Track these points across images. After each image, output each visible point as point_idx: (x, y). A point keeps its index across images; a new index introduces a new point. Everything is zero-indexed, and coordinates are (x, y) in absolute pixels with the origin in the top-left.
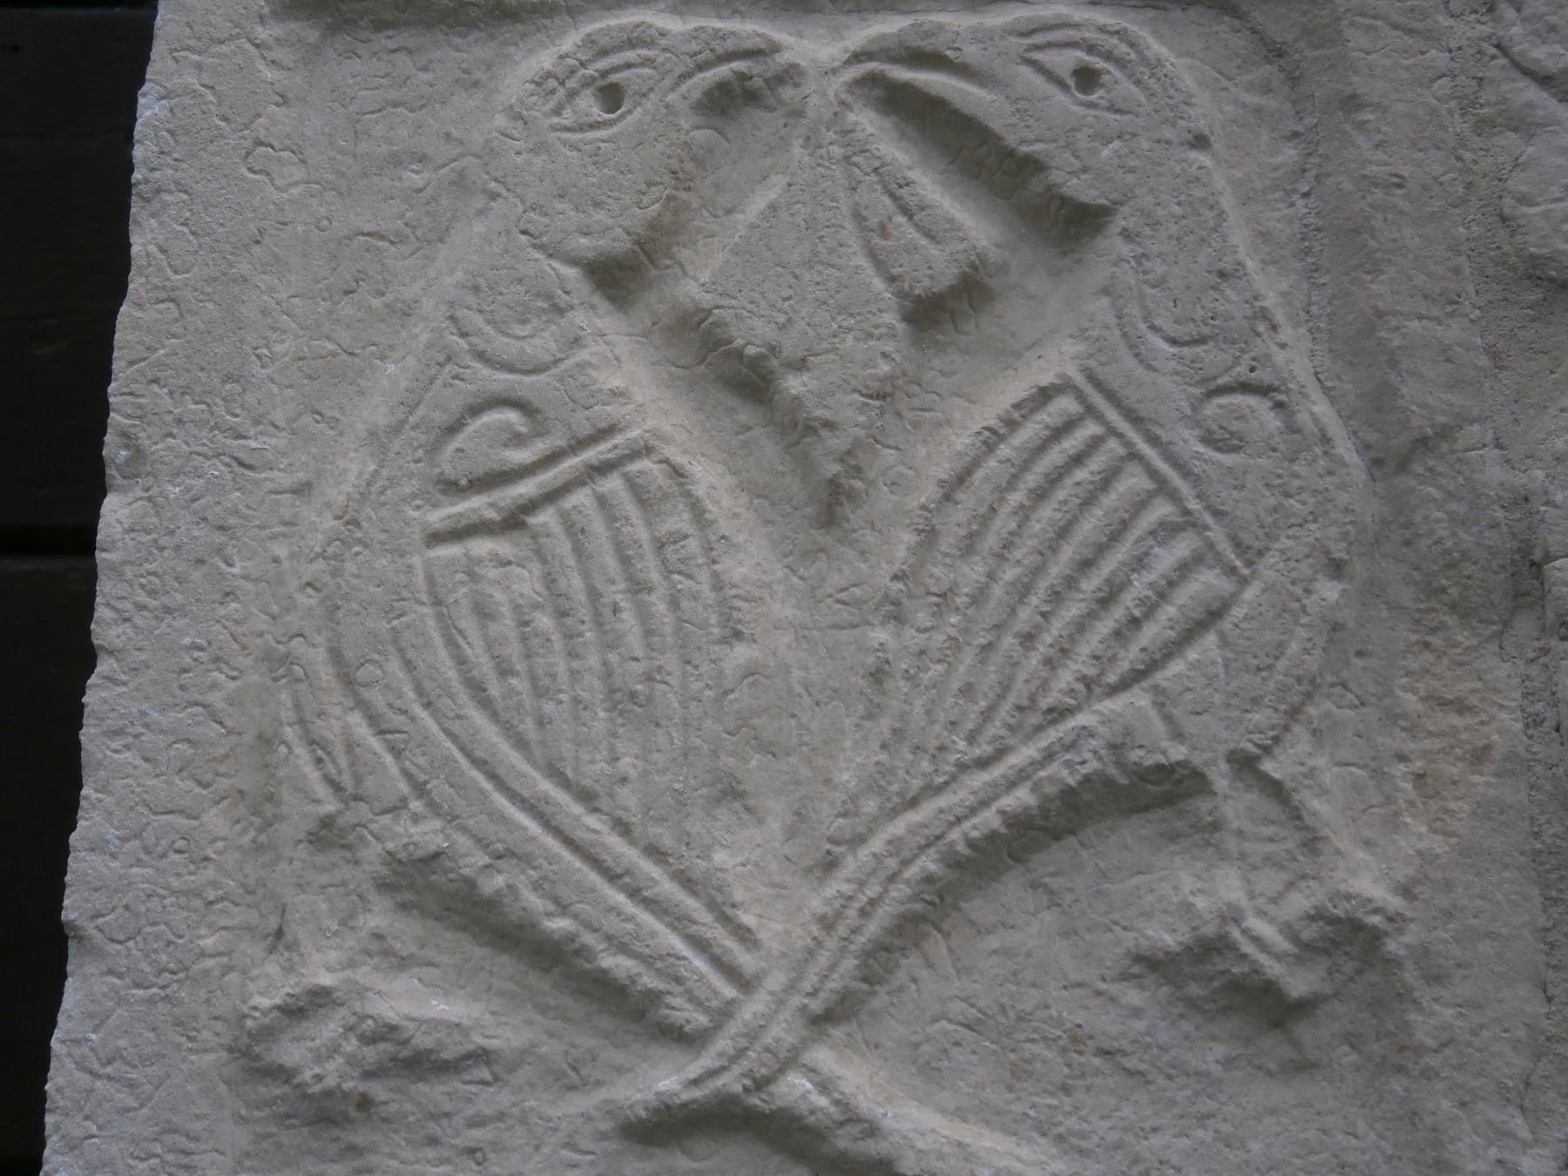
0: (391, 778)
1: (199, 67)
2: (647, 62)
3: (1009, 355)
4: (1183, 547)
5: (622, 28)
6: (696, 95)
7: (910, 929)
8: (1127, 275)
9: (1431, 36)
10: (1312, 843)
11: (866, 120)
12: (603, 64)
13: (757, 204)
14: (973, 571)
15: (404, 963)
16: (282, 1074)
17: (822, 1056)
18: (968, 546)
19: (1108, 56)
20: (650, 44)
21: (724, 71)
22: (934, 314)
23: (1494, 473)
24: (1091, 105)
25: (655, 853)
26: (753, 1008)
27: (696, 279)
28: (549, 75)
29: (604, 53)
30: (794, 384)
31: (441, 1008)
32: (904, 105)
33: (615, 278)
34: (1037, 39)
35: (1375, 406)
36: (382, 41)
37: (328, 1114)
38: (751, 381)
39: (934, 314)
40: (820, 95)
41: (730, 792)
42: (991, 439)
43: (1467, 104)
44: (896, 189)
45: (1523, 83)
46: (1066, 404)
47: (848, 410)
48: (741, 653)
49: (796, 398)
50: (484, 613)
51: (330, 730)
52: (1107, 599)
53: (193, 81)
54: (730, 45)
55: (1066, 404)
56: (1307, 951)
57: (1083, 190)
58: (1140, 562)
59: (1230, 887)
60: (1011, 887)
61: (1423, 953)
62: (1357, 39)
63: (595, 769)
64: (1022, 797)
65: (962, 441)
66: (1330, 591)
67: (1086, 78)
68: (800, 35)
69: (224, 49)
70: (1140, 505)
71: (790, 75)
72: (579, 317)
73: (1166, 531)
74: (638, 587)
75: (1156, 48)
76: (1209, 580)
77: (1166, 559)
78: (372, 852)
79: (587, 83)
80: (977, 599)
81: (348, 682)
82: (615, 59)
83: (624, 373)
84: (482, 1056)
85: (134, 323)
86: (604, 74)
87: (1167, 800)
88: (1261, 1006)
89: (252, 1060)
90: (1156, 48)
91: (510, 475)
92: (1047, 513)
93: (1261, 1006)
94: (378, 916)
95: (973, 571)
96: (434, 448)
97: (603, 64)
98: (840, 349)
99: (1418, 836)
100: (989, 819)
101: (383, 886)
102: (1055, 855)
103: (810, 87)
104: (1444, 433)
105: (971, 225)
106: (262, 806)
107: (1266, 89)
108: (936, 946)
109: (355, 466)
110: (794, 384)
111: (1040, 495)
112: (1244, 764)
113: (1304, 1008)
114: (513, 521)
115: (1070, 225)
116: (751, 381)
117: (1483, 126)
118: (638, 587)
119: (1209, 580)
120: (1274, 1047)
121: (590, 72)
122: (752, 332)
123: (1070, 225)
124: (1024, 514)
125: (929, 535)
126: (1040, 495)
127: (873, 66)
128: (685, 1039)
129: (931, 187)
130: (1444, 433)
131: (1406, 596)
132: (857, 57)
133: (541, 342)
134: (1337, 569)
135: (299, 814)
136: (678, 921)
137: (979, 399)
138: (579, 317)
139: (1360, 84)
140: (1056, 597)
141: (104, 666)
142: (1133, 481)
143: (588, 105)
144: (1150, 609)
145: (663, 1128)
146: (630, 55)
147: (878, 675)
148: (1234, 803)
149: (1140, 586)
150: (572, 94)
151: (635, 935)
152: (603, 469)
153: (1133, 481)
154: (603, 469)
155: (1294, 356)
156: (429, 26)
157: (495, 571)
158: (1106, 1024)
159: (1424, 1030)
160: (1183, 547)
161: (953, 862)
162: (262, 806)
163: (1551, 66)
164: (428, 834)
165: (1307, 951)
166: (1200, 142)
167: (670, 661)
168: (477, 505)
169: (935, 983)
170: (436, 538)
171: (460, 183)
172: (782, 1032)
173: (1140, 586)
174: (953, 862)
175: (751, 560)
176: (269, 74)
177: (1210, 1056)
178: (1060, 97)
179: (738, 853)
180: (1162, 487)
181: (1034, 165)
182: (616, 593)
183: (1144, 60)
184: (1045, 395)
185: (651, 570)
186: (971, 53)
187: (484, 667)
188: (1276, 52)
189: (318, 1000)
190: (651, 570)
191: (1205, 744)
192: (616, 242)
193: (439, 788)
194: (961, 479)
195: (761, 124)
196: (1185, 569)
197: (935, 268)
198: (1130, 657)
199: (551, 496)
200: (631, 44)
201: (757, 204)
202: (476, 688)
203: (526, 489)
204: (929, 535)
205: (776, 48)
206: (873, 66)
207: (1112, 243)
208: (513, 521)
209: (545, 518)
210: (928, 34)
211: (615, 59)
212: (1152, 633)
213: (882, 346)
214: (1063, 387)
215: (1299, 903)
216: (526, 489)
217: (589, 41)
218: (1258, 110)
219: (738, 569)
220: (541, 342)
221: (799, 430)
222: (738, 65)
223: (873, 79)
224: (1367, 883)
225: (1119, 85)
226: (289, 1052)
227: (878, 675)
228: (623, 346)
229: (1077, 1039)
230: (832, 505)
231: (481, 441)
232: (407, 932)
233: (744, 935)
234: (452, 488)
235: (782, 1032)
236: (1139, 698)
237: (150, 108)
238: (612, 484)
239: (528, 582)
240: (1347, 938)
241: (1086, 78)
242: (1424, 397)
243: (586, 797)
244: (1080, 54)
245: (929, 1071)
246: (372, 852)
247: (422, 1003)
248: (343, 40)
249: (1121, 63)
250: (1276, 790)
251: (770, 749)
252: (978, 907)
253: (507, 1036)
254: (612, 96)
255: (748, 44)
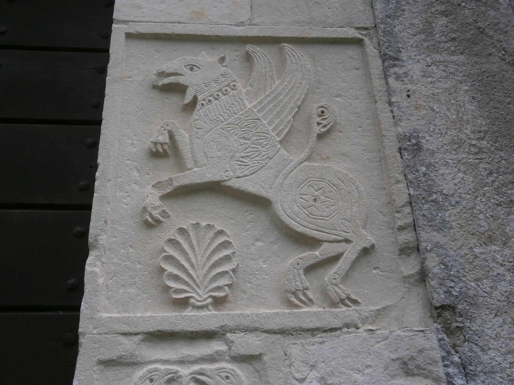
1: (84, 375)
2: (157, 375)
5: (153, 368)
6: (165, 380)
9: (281, 371)
12: (150, 375)
19: (231, 374)
20: (158, 371)
21: (170, 376)
24: (228, 383)
28: (141, 377)
29: (151, 373)
34: (219, 371)
36: (114, 368)
40: (185, 380)
45: (294, 380)
53: (83, 378)
54: (171, 371)
62: (269, 371)
67: (227, 377)
68: (182, 368)
69: (88, 372)
75: (239, 372)
79: (148, 378)
82: (152, 374)
86: (150, 377)
97: (150, 375)
103: (183, 379)
107: (256, 378)
121: (148, 376)
127: (193, 375)
132: (191, 374)
146: (155, 373)
150: (145, 380)
156: (122, 366)
157: (372, 49)
163: (298, 378)
176: (95, 376)
178: (223, 381)
183: (236, 375)
186: (209, 373)
188: (258, 371)
200: (155, 371)
205: (178, 372)
206: (193, 375)
210: (203, 370)
211: (152, 374)
217: (148, 370)
218: (255, 382)
222: (172, 375)
223: (194, 378)
244: (226, 373)
248: (108, 368)
249: (233, 375)
255: (174, 371)
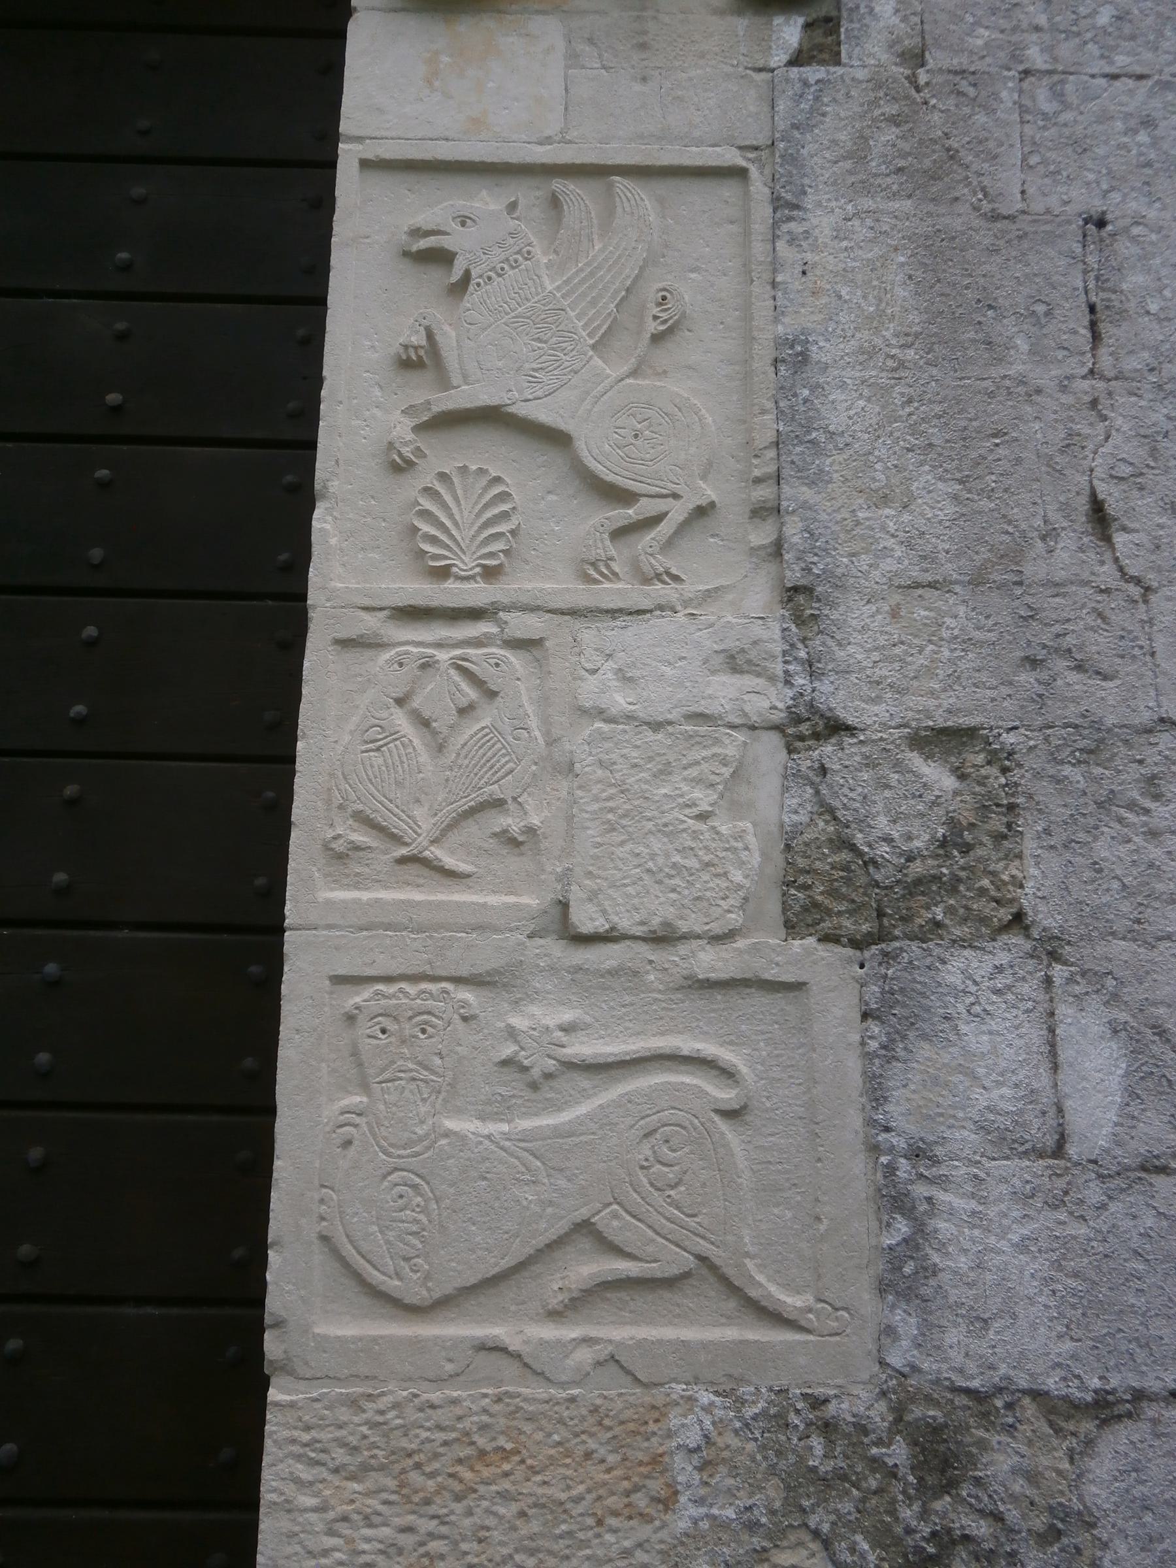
0: (353, 796)
3: (478, 720)
4: (507, 758)
7: (450, 827)
8: (501, 705)
10: (526, 814)
11: (452, 672)
13: (429, 688)
14: (466, 762)
15: (355, 831)
16: (332, 849)
17: (432, 848)
18: (466, 757)
22: (463, 711)
23: (568, 747)
25: (403, 811)
26: (421, 838)
27: (416, 703)
30: (434, 724)
31: (361, 839)
32: (459, 668)
33: (400, 702)
35: (547, 734)
37: (340, 857)
38: (426, 723)
39: (463, 711)
40: (443, 666)
41: (418, 801)
42: (472, 737)
43: (572, 674)
44: (457, 686)
46: (487, 730)
47: (445, 731)
48: (421, 775)
49: (912, 751)
50: (372, 766)
51: (342, 787)
52: (491, 768)
54: (424, 1009)
55: (487, 730)
56: (523, 833)
57: (494, 688)
58: (498, 761)
59: (510, 821)
60: (470, 821)
61: (544, 833)
62: (551, 660)
63: (392, 796)
64: (473, 803)
65: (466, 737)
66: (534, 768)
67: (497, 665)
70: (500, 750)
71: (437, 662)
72: (392, 710)
73: (504, 755)
74: (402, 762)
75: (512, 659)
76: (511, 765)
77: (503, 760)
78: (350, 810)
80: (467, 766)
81: (345, 778)
83: (400, 720)
84: (369, 847)
85: (303, 707)
87: (500, 805)
88: (514, 843)
89: (326, 847)
90: (512, 659)
91: (378, 740)
92: (482, 751)
93: (514, 843)
94: (350, 822)
95: (466, 762)
96: (363, 735)
98: (444, 718)
99: (546, 813)
100: (466, 807)
101: (352, 817)
102: (477, 816)
104: (559, 739)
105: (471, 693)
106: (328, 802)
108: (456, 831)
109: (347, 738)
110: (434, 724)
111: (480, 747)
112: (514, 799)
113: (522, 843)
114: (378, 749)
115: (492, 695)
116: (426, 723)
117: (574, 679)
118: (402, 762)
119: (511, 765)
120: (516, 851)
122: (426, 714)
123: (492, 695)
124: (477, 751)
125: (458, 754)
126: (480, 747)
128: (407, 844)
129: (464, 686)
130: (559, 739)
131: (550, 769)
133: (385, 714)
134: (536, 764)
135: (336, 803)
136: (407, 824)
137: (471, 728)
138: (392, 710)
139: (551, 669)
140: (482, 767)
141: (298, 775)
142: (499, 745)
143: (396, 666)
144: (499, 770)
145: (402, 861)
147: (447, 780)
148: (511, 806)
149: (498, 765)
151: (398, 826)
152: (396, 739)
153: (499, 745)
154: (396, 739)
155: (533, 723)
158: (486, 845)
159: (542, 847)
160: (507, 758)
161: (459, 815)
162: (328, 802)
164: (360, 807)
165: (523, 833)
166: (518, 679)
167: (407, 776)
168: (371, 746)
169: (454, 837)
170: (363, 752)
171: (369, 680)
172: (425, 843)
173: (498, 765)
174: (459, 815)
175: (424, 758)
177: (504, 852)
179: (418, 812)
180: (504, 747)
181: (485, 682)
182: (398, 763)
184: (483, 728)
185: (405, 759)
186: (474, 659)
187: (372, 776)
189: (339, 836)
190: (405, 759)
191: (507, 795)
192: (401, 695)
193: (363, 799)
194: (465, 744)
195: (431, 671)
196: (507, 762)
197: (464, 702)
198: (495, 778)
199: (385, 745)
201: (429, 688)
202: (370, 780)
203: (381, 743)
204: (458, 754)
207: (499, 699)
208: (378, 749)
209: (384, 748)
212: (499, 774)
213: (452, 717)
214: (487, 727)
215: (522, 824)
216: (381, 743)
219: (421, 760)
220: (385, 714)
221: (435, 733)
224: (535, 821)
225: (503, 667)
226: (333, 846)
227: (447, 780)
228: (401, 715)
229: (480, 848)
230: (441, 748)
231: (373, 733)
232: (356, 825)
233: (419, 826)
234: (367, 742)
235: (425, 843)
236: (496, 786)
237: (306, 664)
238: (398, 742)
239: (381, 761)
240: (530, 831)
241: (497, 665)
242: (556, 732)
243: (391, 801)
245: (452, 852)
246: (350, 810)
247: (358, 838)
250: (520, 804)
251: (426, 794)
252: (464, 824)
253: (374, 844)
254: (401, 665)
